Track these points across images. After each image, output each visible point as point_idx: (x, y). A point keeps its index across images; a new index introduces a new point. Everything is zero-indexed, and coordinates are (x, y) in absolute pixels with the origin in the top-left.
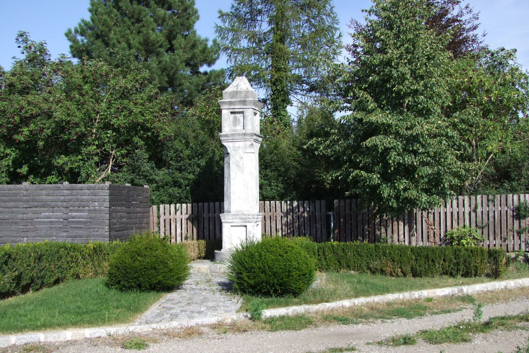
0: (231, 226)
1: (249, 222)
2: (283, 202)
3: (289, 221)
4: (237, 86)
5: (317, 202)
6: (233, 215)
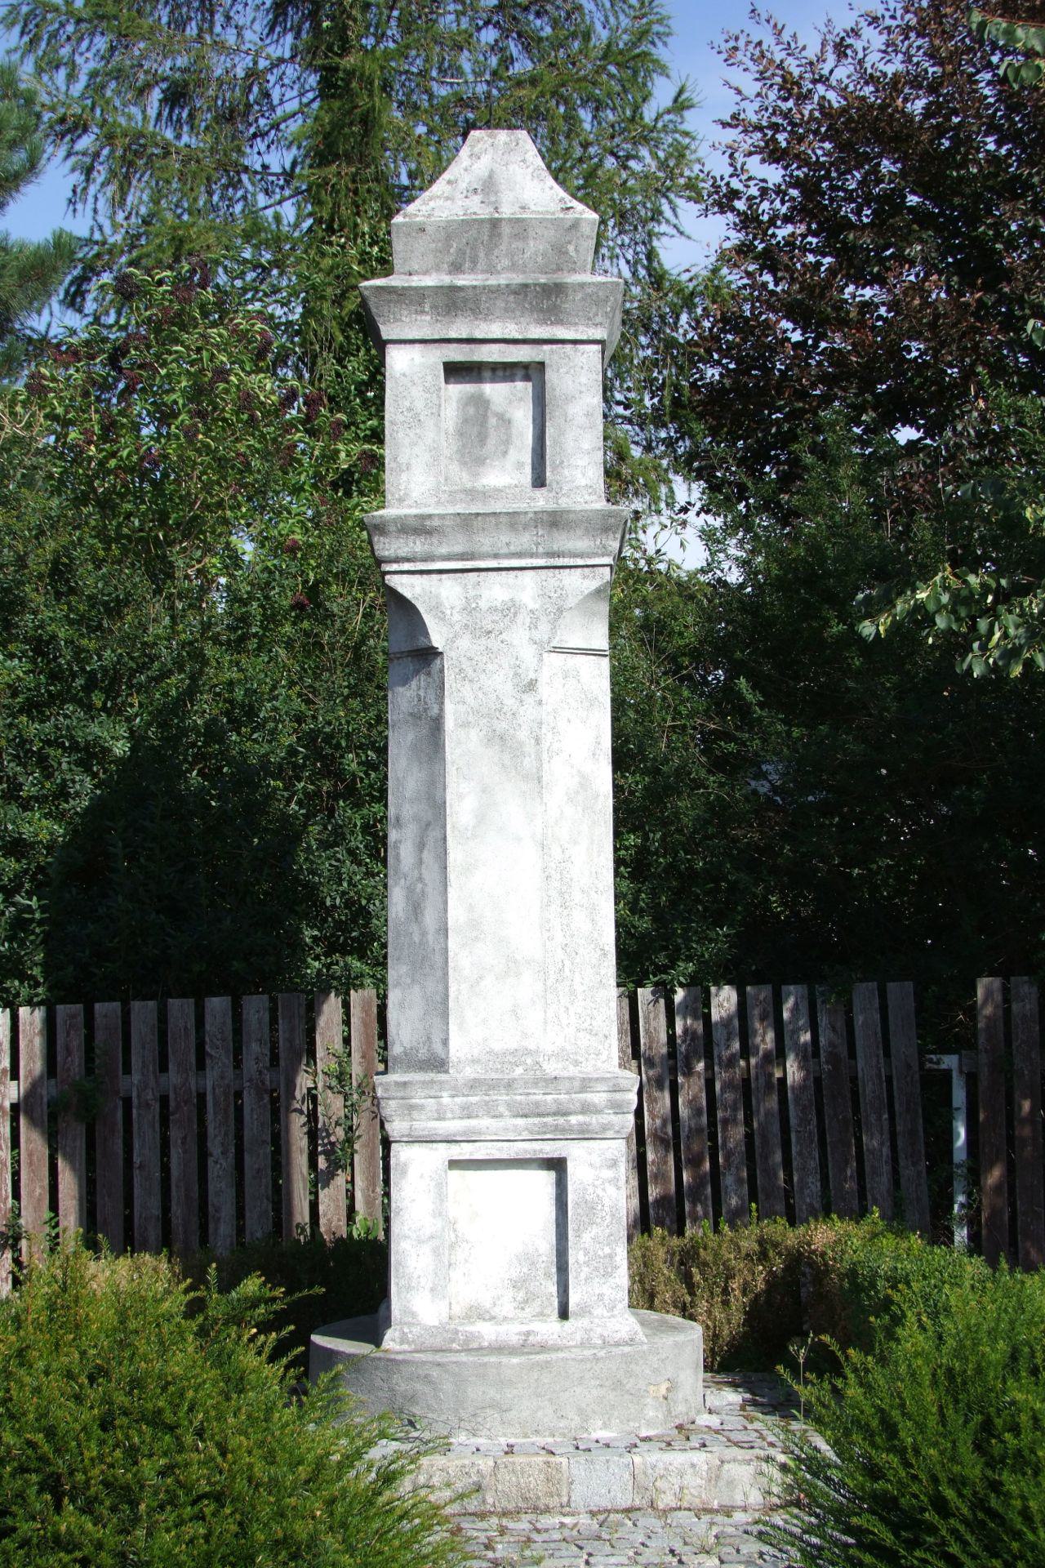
0: (454, 1164)
1: (585, 1135)
2: (644, 994)
3: (684, 1112)
4: (488, 187)
5: (864, 994)
6: (474, 1085)
